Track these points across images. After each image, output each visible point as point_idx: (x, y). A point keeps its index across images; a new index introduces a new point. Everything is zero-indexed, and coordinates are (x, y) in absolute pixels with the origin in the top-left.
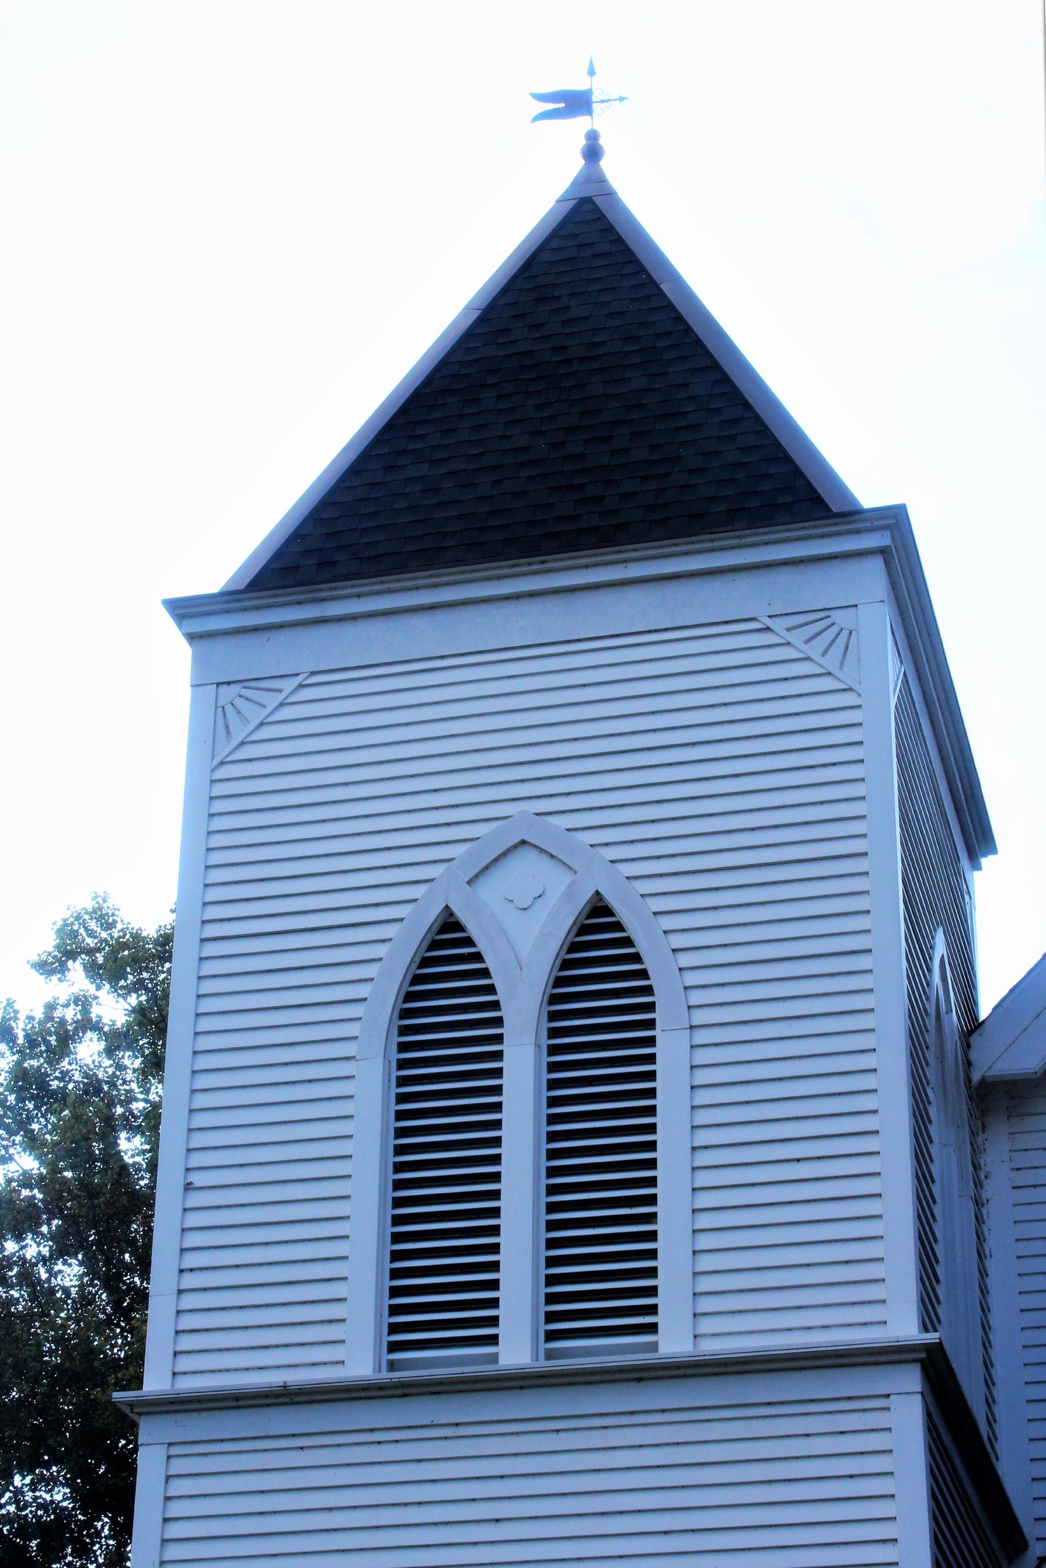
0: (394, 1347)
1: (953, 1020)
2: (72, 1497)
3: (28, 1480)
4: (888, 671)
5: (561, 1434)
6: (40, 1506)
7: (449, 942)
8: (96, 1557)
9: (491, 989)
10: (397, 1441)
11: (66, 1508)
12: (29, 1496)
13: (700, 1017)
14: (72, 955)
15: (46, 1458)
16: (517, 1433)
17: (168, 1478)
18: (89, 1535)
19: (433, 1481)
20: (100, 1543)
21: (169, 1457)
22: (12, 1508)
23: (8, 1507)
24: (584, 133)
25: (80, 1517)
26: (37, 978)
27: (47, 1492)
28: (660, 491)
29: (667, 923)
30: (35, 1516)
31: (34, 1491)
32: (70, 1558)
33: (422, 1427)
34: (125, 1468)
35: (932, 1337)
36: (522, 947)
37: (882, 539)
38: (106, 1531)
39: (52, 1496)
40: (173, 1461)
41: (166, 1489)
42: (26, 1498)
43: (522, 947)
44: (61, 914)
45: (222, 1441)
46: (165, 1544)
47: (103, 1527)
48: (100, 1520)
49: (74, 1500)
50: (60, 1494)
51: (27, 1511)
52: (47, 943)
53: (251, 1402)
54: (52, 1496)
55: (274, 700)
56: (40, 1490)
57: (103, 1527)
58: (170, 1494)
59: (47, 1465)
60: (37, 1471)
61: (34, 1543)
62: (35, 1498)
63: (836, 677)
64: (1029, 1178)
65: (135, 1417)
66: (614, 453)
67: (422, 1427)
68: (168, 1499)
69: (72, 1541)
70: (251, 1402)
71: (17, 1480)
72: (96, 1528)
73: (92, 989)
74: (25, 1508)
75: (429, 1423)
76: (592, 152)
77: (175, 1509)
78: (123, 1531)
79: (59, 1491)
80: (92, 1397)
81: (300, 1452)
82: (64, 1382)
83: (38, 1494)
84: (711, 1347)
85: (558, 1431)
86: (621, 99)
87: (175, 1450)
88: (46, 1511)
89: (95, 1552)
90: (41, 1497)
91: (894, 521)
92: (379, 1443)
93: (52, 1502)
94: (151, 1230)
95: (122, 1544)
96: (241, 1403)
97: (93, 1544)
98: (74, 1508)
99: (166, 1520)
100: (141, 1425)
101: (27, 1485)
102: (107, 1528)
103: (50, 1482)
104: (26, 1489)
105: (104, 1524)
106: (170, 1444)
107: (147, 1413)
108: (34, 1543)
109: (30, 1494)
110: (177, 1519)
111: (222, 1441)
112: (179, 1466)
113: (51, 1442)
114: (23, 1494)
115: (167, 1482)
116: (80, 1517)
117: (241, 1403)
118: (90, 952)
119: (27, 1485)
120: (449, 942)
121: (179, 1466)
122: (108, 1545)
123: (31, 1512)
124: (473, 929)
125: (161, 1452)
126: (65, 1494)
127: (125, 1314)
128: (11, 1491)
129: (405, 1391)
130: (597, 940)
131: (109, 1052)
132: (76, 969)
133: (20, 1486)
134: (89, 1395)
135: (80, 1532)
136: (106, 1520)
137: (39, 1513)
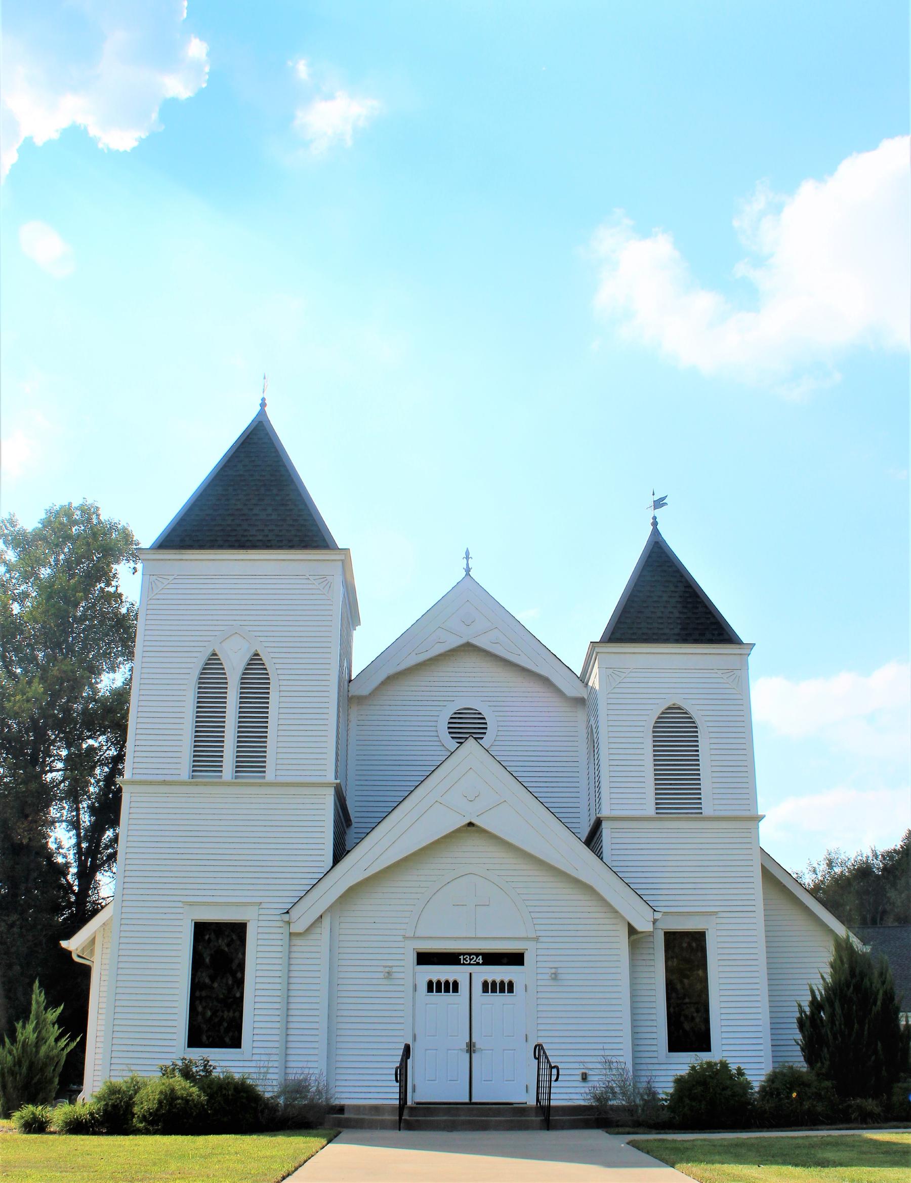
7: (213, 664)
9: (226, 678)
13: (282, 688)
24: (71, 495)
28: (280, 531)
35: (338, 781)
36: (234, 666)
37: (343, 557)
43: (234, 666)
55: (166, 582)
64: (362, 723)
66: (267, 515)
86: (467, 557)
91: (346, 551)
94: (8, 997)
120: (213, 664)
124: (220, 656)
130: (255, 662)
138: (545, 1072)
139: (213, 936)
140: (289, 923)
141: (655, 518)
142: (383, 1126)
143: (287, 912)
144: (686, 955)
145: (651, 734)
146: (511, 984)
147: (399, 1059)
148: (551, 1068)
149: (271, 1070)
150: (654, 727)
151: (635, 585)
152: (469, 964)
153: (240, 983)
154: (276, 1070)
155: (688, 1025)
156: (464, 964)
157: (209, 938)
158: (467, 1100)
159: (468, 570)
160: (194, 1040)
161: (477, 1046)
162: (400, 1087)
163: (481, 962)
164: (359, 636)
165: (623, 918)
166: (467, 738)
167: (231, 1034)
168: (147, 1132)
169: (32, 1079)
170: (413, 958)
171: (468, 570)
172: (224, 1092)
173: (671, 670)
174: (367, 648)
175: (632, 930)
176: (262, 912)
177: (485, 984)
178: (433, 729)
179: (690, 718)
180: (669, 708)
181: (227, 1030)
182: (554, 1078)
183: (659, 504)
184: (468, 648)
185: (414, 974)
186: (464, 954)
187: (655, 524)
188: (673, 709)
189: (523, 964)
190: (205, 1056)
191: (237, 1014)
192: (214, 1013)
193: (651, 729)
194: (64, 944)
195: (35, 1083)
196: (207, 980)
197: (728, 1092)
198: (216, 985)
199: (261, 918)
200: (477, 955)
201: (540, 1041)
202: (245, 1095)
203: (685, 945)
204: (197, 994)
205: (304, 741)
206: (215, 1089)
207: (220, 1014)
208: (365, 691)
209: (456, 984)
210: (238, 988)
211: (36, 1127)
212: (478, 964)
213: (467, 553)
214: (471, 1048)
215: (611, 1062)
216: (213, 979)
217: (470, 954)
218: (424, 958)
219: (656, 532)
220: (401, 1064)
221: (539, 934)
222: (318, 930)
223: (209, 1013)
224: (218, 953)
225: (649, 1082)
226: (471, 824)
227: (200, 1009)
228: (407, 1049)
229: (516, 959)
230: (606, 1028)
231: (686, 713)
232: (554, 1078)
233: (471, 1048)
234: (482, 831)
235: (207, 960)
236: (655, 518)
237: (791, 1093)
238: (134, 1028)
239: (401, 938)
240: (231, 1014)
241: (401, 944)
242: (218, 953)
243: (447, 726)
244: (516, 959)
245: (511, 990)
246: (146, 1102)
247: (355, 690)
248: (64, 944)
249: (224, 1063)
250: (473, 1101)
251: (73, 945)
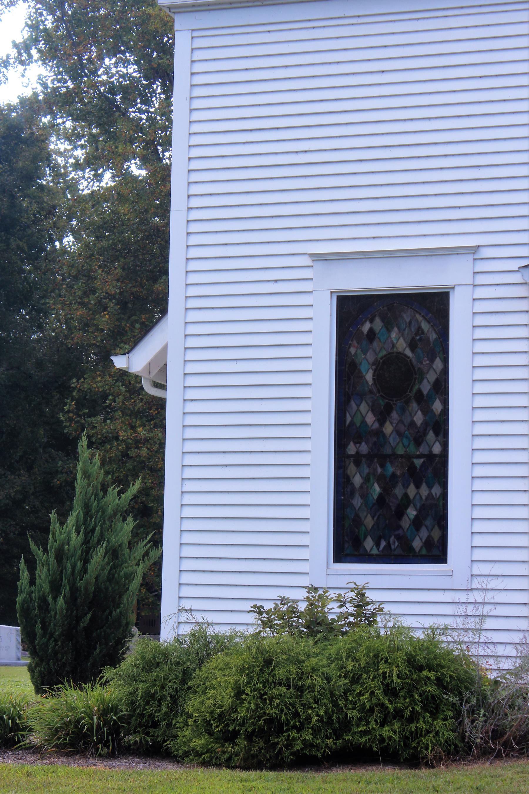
2: (138, 71)
3: (113, 60)
5: (419, 21)
6: (121, 76)
8: (154, 105)
10: (324, 27)
11: (136, 77)
12: (114, 70)
15: (123, 48)
16: (394, 21)
17: (193, 50)
18: (149, 92)
19: (345, 50)
20: (156, 96)
21: (192, 38)
22: (105, 77)
23: (103, 76)
25: (144, 82)
27: (125, 67)
30: (118, 82)
31: (116, 67)
32: (139, 105)
33: (339, 18)
34: (168, 51)
38: (159, 90)
39: (127, 70)
40: (195, 40)
41: (191, 56)
42: (112, 71)
45: (223, 28)
46: (193, 87)
47: (157, 87)
48: (155, 84)
49: (139, 71)
50: (132, 69)
51: (113, 79)
53: (239, 5)
54: (127, 70)
56: (120, 67)
57: (157, 87)
58: (194, 59)
59: (123, 53)
60: (118, 56)
61: (118, 97)
62: (117, 72)
65: (172, 15)
67: (339, 18)
68: (193, 62)
69: (140, 95)
70: (239, 5)
71: (107, 61)
72: (153, 88)
74: (112, 77)
75: (342, 15)
77: (198, 67)
78: (168, 90)
79: (118, 404)
80: (147, 12)
81: (268, 34)
82: (130, 3)
83: (119, 69)
85: (418, 19)
87: (195, 34)
88: (124, 79)
89: (153, 102)
90: (121, 71)
92: (314, 28)
93: (128, 74)
95: (169, 97)
96: (233, 6)
97: (152, 97)
98: (140, 77)
99: (192, 74)
100: (177, 27)
101: (112, 64)
102: (159, 88)
103: (126, 63)
104: (112, 66)
105: (157, 86)
106: (193, 30)
107: (179, 12)
108: (118, 97)
109: (115, 69)
110: (199, 73)
111: (223, 28)
112: (199, 43)
113: (125, 39)
114: (110, 69)
115: (192, 53)
116: (144, 82)
117: (233, 6)
119: (112, 64)
121: (199, 43)
122: (160, 98)
123: (116, 79)
125: (188, 35)
126: (134, 69)
127: (148, 441)
128: (104, 68)
133: (108, 64)
134: (145, 11)
135: (144, 90)
136: (159, 84)
137: (121, 80)
139: (378, 324)
153: (440, 426)
157: (371, 330)
160: (348, 546)
167: (424, 533)
168: (209, 760)
169: (78, 619)
172: (383, 667)
176: (481, 266)
181: (417, 523)
189: (446, 563)
190: (361, 582)
191: (436, 490)
192: (387, 490)
194: (119, 362)
195: (85, 629)
196: (370, 419)
198: (388, 429)
199: (481, 279)
202: (432, 675)
204: (352, 449)
206: (363, 663)
207: (399, 491)
210: (437, 434)
216: (383, 416)
223: (377, 489)
224: (391, 366)
227: (357, 480)
235: (369, 377)
237: (134, 44)
240: (424, 491)
242: (391, 366)
246: (215, 691)
248: (119, 362)
249: (406, 599)
251: (135, 361)
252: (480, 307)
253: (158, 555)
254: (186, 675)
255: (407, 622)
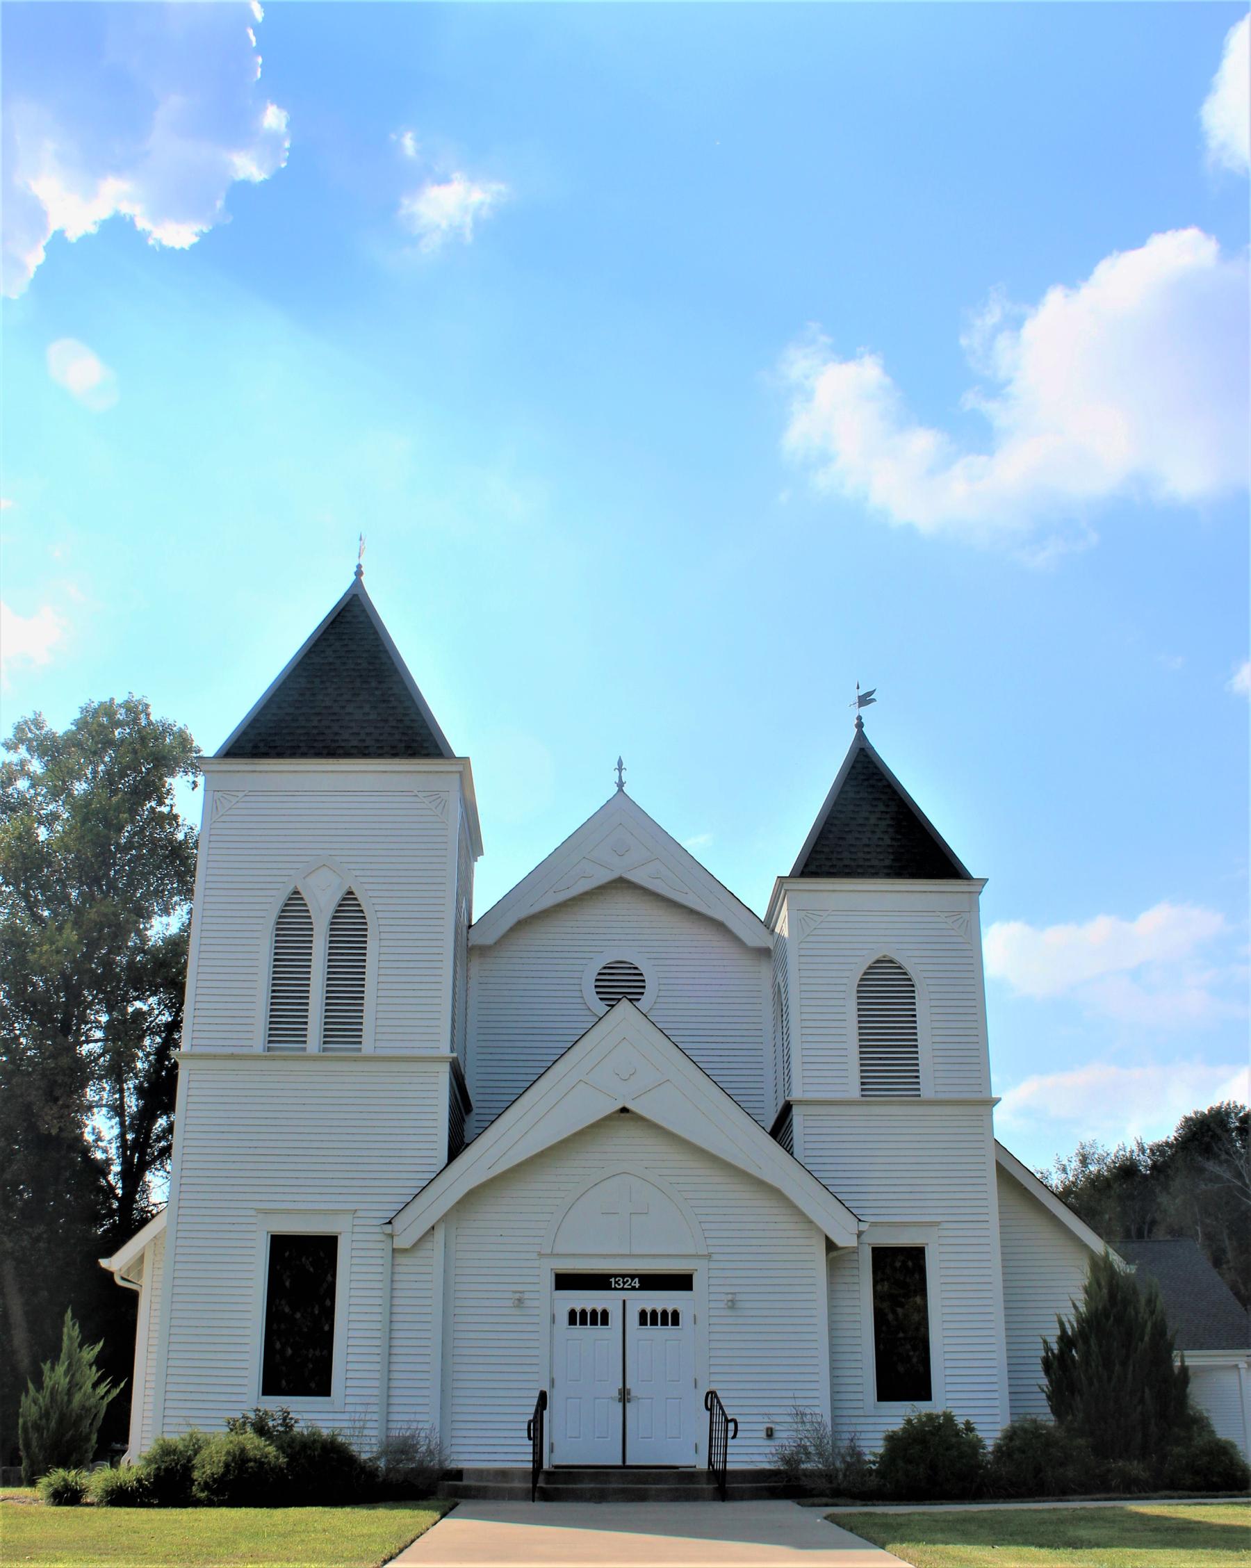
0: (270, 1042)
1: (466, 923)
4: (456, 811)
14: (22, 741)
26: (3, 750)
29: (370, 894)
35: (455, 1055)
37: (460, 768)
44: (18, 719)
52: (9, 734)
55: (234, 800)
63: (551, 1372)
73: (29, 757)
76: (359, 573)
84: (380, 1052)
86: (620, 768)
118: (30, 740)
129: (274, 1059)
131: (33, 786)
132: (23, 750)
138: (719, 1427)
140: (391, 1236)
141: (859, 718)
142: (512, 1495)
143: (390, 1223)
144: (900, 1277)
145: (855, 995)
146: (676, 1314)
147: (533, 1410)
148: (727, 1421)
149: (369, 1425)
150: (859, 986)
151: (835, 804)
152: (623, 1289)
154: (376, 1425)
155: (903, 1364)
156: (616, 1289)
158: (620, 1463)
159: (621, 784)
160: (271, 1387)
161: (633, 1394)
162: (534, 1445)
163: (637, 1285)
164: (481, 868)
165: (819, 1230)
166: (619, 1000)
168: (210, 1503)
170: (550, 1281)
171: (621, 784)
173: (881, 912)
174: (491, 884)
175: (830, 1246)
176: (357, 1222)
177: (643, 1314)
178: (577, 987)
179: (905, 974)
180: (878, 961)
182: (731, 1434)
183: (865, 700)
184: (621, 884)
185: (552, 1301)
186: (616, 1276)
187: (860, 725)
188: (884, 963)
190: (285, 1406)
193: (855, 988)
194: (104, 1263)
196: (287, 1310)
197: (955, 1453)
199: (356, 1229)
200: (633, 1277)
201: (713, 1387)
203: (898, 1264)
205: (410, 1003)
208: (489, 940)
209: (605, 1314)
211: (68, 1497)
212: (634, 1289)
213: (620, 763)
214: (625, 1396)
215: (803, 1414)
217: (623, 1276)
218: (565, 1281)
219: (861, 737)
220: (535, 1417)
221: (711, 1250)
222: (429, 1245)
224: (302, 1275)
225: (852, 1440)
226: (624, 1110)
227: (278, 1346)
228: (543, 1397)
229: (682, 1282)
230: (795, 1370)
231: (899, 968)
232: (731, 1434)
233: (625, 1396)
234: (640, 1119)
236: (859, 718)
238: (193, 1369)
239: (534, 1256)
241: (536, 1264)
242: (302, 1275)
243: (593, 984)
244: (682, 1282)
245: (676, 1322)
246: (207, 1467)
247: (476, 939)
248: (104, 1263)
249: (308, 1415)
250: (628, 1463)
252: (355, 1245)
253: (879, 1287)
254: (190, 1460)
255: (319, 1424)
